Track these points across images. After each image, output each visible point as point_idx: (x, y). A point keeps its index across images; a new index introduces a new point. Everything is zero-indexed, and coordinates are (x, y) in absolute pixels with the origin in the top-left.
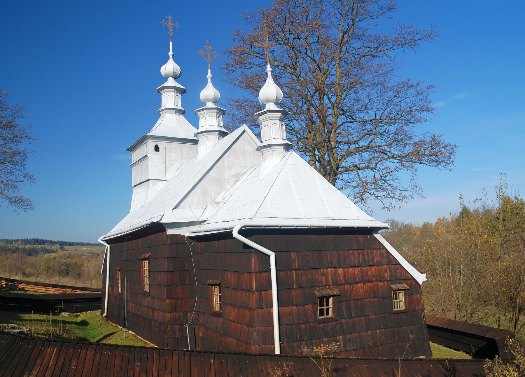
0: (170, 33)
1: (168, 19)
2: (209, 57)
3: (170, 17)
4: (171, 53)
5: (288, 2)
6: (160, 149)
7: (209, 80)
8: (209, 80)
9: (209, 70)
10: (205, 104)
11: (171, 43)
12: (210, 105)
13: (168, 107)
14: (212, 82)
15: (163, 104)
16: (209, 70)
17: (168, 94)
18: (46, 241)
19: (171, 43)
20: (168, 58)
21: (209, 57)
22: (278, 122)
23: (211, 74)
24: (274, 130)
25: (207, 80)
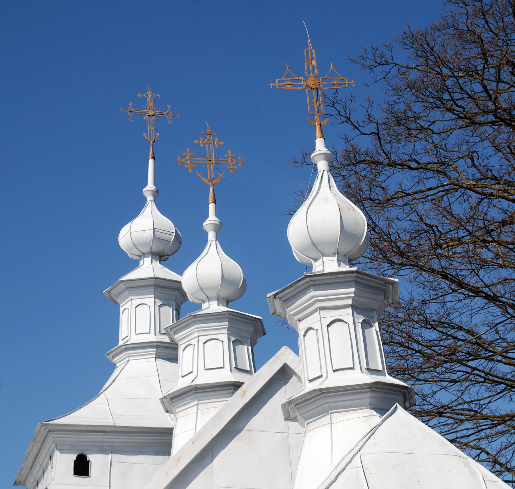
0: (150, 133)
1: (144, 100)
2: (210, 169)
3: (150, 94)
4: (150, 186)
5: (508, 188)
6: (93, 469)
7: (211, 235)
8: (211, 235)
9: (212, 207)
10: (199, 307)
11: (151, 162)
12: (214, 307)
13: (135, 339)
14: (218, 238)
15: (123, 331)
16: (212, 207)
17: (135, 302)
18: (505, 364)
19: (151, 162)
20: (143, 202)
21: (210, 169)
22: (347, 314)
23: (217, 215)
24: (333, 344)
25: (207, 234)
